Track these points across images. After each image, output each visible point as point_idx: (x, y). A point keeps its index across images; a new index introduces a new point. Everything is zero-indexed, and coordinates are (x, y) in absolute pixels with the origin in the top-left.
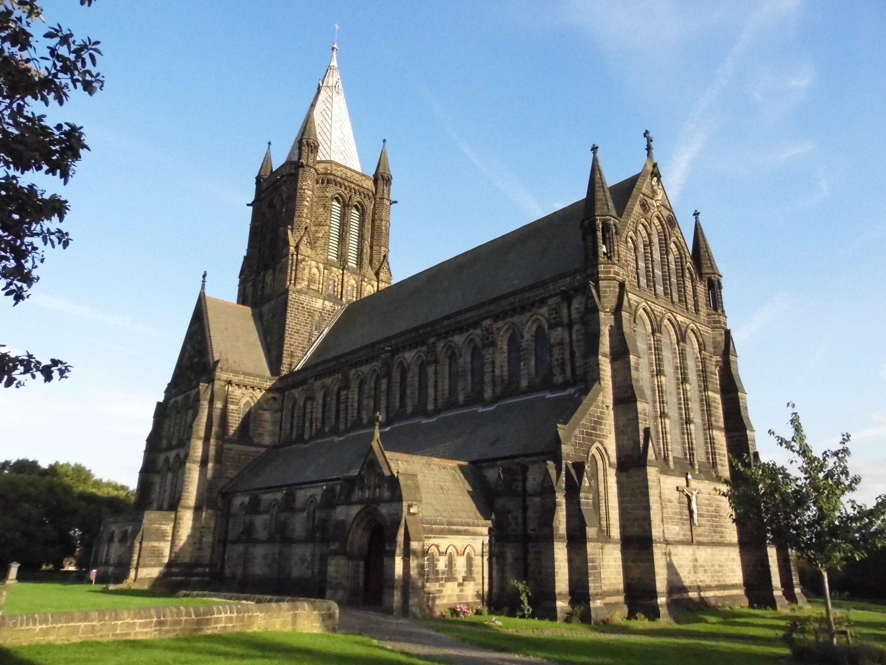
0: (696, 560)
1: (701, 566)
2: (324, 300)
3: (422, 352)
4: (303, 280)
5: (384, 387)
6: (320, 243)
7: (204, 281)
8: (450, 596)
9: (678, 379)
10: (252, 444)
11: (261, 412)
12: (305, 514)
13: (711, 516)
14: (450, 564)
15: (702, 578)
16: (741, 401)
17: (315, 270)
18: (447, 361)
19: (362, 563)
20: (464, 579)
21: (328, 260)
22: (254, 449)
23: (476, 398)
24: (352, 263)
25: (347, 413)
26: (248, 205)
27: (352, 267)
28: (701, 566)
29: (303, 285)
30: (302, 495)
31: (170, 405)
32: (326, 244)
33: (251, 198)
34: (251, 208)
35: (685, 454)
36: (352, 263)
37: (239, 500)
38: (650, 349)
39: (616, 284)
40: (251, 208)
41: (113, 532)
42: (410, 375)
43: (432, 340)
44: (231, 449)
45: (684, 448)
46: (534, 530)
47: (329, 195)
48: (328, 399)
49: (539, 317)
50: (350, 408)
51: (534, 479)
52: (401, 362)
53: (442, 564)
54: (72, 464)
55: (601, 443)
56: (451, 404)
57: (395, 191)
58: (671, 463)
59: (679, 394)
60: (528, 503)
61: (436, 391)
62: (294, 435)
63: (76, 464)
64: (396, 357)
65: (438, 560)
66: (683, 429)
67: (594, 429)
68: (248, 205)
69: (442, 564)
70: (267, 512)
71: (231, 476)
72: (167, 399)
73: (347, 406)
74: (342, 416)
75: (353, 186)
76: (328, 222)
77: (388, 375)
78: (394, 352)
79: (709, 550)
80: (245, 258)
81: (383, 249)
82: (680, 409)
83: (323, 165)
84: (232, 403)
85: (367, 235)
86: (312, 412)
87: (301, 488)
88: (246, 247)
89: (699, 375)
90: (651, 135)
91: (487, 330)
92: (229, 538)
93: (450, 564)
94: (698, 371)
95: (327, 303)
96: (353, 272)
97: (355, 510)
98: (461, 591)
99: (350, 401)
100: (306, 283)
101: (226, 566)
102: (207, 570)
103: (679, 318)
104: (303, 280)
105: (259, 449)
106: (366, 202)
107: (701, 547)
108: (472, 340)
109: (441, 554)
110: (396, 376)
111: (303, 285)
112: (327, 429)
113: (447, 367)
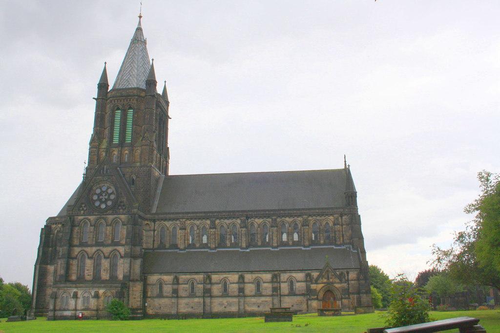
54: (412, 278)
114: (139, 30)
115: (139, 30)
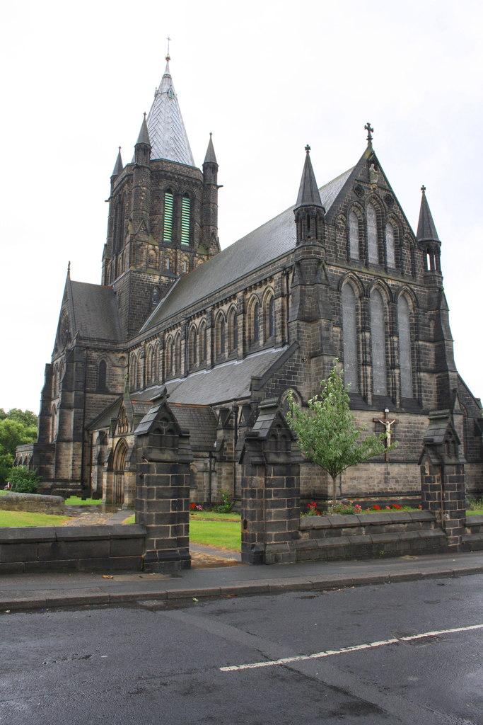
0: (388, 473)
1: (393, 478)
2: (160, 276)
7: (69, 269)
9: (386, 332)
10: (107, 392)
11: (114, 368)
13: (410, 440)
15: (393, 487)
16: (447, 347)
17: (152, 252)
18: (220, 325)
22: (110, 397)
24: (185, 242)
26: (106, 201)
28: (393, 478)
29: (142, 265)
34: (108, 203)
35: (389, 393)
36: (185, 242)
38: (357, 310)
39: (314, 261)
44: (92, 398)
45: (388, 388)
47: (162, 188)
54: (24, 411)
55: (295, 389)
57: (221, 178)
58: (370, 401)
59: (386, 344)
61: (212, 349)
63: (27, 411)
66: (388, 373)
67: (289, 378)
68: (106, 201)
71: (94, 417)
75: (182, 178)
76: (162, 211)
78: (189, 320)
79: (403, 466)
80: (106, 245)
81: (211, 227)
82: (387, 357)
84: (91, 363)
85: (197, 218)
86: (144, 367)
88: (106, 236)
89: (411, 328)
90: (371, 127)
94: (411, 324)
95: (163, 278)
96: (184, 250)
102: (79, 484)
103: (390, 282)
105: (115, 396)
106: (195, 190)
114: (167, 77)
115: (167, 77)
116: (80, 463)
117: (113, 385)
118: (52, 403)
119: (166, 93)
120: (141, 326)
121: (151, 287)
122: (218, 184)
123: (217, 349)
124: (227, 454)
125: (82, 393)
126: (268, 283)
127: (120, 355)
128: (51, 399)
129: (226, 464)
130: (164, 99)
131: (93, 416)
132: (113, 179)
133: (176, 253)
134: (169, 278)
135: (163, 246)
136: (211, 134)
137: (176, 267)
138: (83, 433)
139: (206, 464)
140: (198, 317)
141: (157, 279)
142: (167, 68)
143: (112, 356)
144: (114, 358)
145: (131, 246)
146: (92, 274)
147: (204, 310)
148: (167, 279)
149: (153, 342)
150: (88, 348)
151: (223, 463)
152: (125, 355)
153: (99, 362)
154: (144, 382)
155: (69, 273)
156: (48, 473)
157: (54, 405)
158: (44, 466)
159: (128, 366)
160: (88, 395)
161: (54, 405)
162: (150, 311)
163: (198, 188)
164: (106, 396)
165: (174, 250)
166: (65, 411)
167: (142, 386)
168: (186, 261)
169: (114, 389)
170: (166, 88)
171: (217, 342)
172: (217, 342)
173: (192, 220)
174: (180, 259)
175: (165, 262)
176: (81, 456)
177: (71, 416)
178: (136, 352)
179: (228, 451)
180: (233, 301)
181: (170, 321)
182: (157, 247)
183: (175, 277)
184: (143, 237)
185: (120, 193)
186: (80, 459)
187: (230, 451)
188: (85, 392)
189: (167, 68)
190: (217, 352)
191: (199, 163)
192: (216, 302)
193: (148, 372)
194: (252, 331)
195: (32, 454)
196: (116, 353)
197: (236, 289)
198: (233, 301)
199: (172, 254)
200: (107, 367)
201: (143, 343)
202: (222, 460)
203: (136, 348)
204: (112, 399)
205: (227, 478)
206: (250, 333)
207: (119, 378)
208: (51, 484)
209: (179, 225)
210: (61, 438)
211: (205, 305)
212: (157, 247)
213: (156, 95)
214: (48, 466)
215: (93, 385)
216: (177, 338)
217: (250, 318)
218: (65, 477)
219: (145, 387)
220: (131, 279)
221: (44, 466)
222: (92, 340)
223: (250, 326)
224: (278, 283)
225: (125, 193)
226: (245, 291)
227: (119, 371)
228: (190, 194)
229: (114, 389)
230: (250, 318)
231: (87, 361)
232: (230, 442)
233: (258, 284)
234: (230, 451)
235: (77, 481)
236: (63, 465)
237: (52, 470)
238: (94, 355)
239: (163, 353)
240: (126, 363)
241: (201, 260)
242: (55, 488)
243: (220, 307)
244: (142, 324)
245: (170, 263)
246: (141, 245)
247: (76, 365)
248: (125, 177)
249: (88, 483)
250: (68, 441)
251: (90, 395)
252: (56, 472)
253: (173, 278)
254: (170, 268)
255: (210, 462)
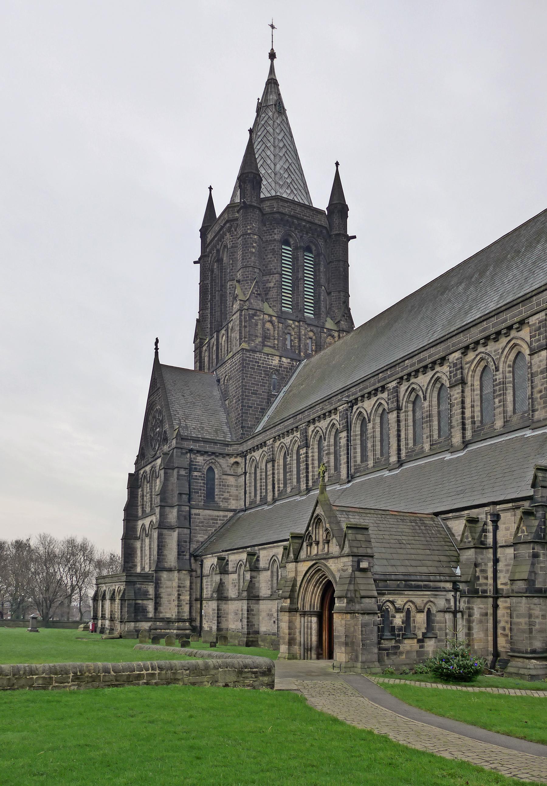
3: (382, 398)
4: (256, 336)
5: (343, 442)
6: (273, 293)
7: (157, 349)
8: (408, 652)
10: (219, 509)
11: (225, 477)
12: (269, 573)
14: (407, 620)
18: (410, 406)
19: (314, 619)
20: (424, 634)
21: (282, 312)
22: (221, 513)
23: (443, 445)
25: (307, 472)
26: (195, 262)
27: (309, 318)
29: (257, 342)
30: (264, 556)
31: (140, 476)
32: (280, 294)
33: (197, 254)
34: (198, 265)
36: (309, 315)
37: (210, 561)
40: (198, 265)
41: (105, 591)
42: (370, 426)
43: (394, 384)
44: (199, 515)
46: (505, 584)
48: (289, 459)
49: (519, 342)
50: (310, 466)
51: (507, 529)
52: (360, 413)
53: (398, 620)
56: (413, 456)
60: (499, 555)
62: (258, 498)
64: (355, 407)
65: (395, 617)
68: (195, 262)
69: (398, 620)
70: (235, 572)
71: (201, 539)
72: (137, 470)
73: (307, 465)
74: (303, 475)
77: (348, 428)
80: (198, 321)
83: (268, 203)
84: (196, 470)
87: (264, 548)
91: (455, 365)
92: (205, 596)
93: (407, 620)
95: (284, 359)
97: (303, 567)
98: (422, 647)
99: (310, 459)
100: (260, 339)
101: (204, 622)
104: (256, 336)
105: (226, 513)
107: (453, 532)
108: (438, 379)
109: (398, 610)
110: (356, 429)
111: (257, 342)
112: (289, 490)
113: (410, 413)
114: (272, 83)
115: (272, 83)
116: (188, 598)
117: (224, 499)
118: (140, 523)
119: (271, 104)
120: (259, 423)
121: (268, 372)
122: (350, 233)
123: (407, 439)
124: (481, 585)
125: (187, 508)
126: (332, 414)
127: (233, 460)
128: (137, 519)
129: (479, 599)
130: (270, 114)
131: (201, 537)
132: (204, 232)
133: (299, 327)
134: (292, 359)
135: (282, 317)
136: (337, 164)
137: (300, 346)
138: (190, 560)
139: (448, 601)
140: (369, 398)
141: (276, 361)
142: (272, 70)
143: (221, 461)
144: (225, 463)
145: (241, 315)
146: (181, 354)
147: (297, 427)
148: (289, 360)
149: (287, 440)
150: (191, 451)
151: (476, 600)
152: (239, 459)
153: (206, 467)
154: (274, 493)
155: (157, 354)
156: (144, 610)
157: (143, 525)
158: (140, 602)
159: (245, 473)
160: (194, 511)
161: (143, 525)
162: (269, 403)
163: (324, 236)
164: (216, 513)
165: (297, 323)
166: (165, 532)
167: (270, 498)
168: (311, 338)
169: (226, 504)
170: (272, 98)
171: (406, 430)
172: (406, 430)
173: (317, 284)
174: (305, 335)
175: (285, 339)
176: (188, 589)
177: (172, 540)
178: (257, 455)
179: (482, 581)
180: (295, 434)
181: (318, 408)
182: (274, 318)
183: (298, 358)
184: (257, 304)
185: (218, 247)
186: (188, 593)
187: (485, 581)
188: (190, 508)
189: (272, 70)
190: (407, 444)
191: (321, 200)
192: (406, 372)
193: (279, 480)
194: (477, 409)
195: (122, 588)
196: (227, 458)
197: (448, 347)
198: (295, 434)
199: (293, 329)
200: (217, 476)
201: (268, 443)
202: (475, 593)
203: (258, 449)
204: (224, 516)
205: (481, 622)
206: (473, 412)
207: (233, 491)
208: (149, 624)
209: (301, 288)
210: (160, 566)
211: (385, 379)
212: (274, 318)
213: (258, 110)
214: (145, 602)
215: (199, 498)
216: (330, 431)
217: (473, 390)
218: (168, 615)
219: (274, 500)
220: (243, 360)
221: (140, 602)
222: (196, 440)
223: (473, 401)
224: (392, 393)
225: (226, 246)
226: (466, 350)
227: (231, 480)
228: (314, 248)
229: (226, 504)
230: (473, 390)
231: (191, 468)
232: (483, 568)
233: (405, 377)
234: (485, 581)
235: (184, 621)
236: (164, 600)
237: (150, 607)
238: (200, 459)
239: (307, 453)
240: (240, 470)
241: (329, 337)
242: (156, 629)
243: (413, 380)
244: (258, 421)
245: (291, 340)
246: (255, 315)
247: (178, 472)
248: (225, 224)
249: (198, 624)
250: (170, 570)
251: (197, 511)
252: (156, 609)
253: (297, 360)
254: (291, 346)
255: (455, 597)
